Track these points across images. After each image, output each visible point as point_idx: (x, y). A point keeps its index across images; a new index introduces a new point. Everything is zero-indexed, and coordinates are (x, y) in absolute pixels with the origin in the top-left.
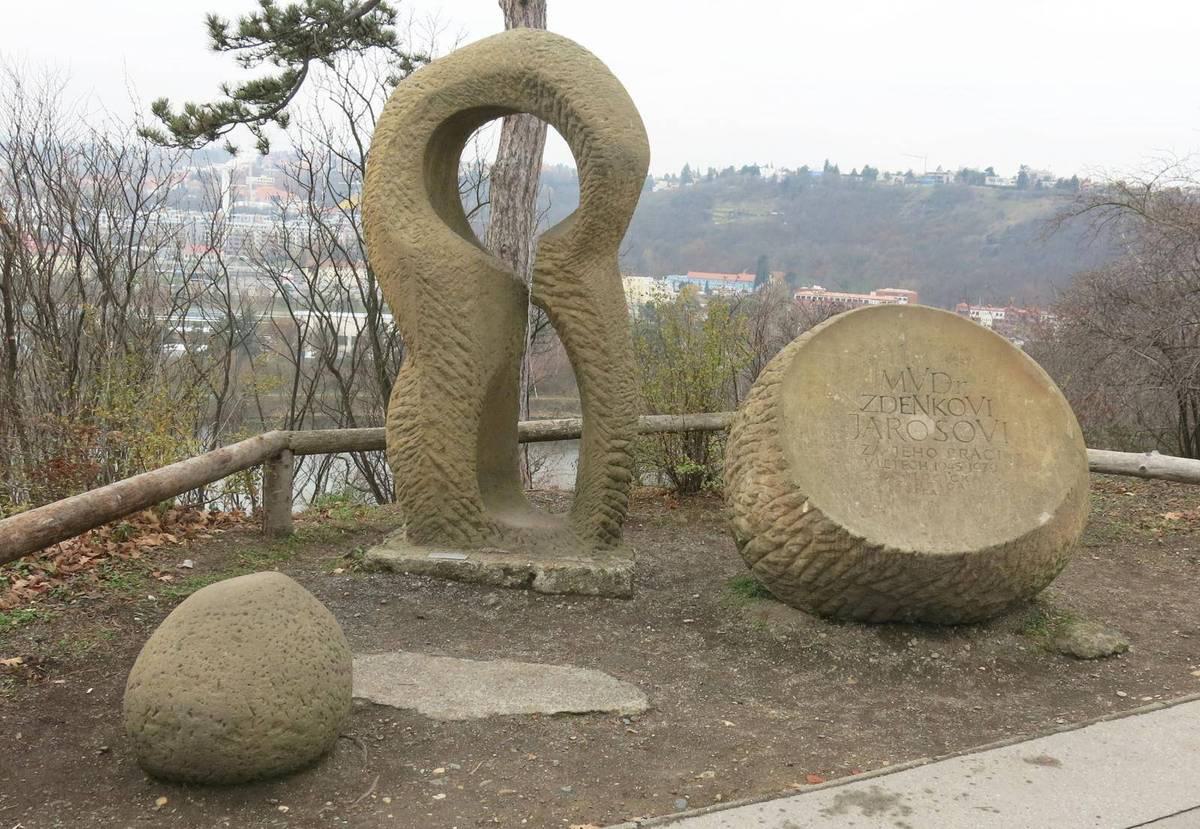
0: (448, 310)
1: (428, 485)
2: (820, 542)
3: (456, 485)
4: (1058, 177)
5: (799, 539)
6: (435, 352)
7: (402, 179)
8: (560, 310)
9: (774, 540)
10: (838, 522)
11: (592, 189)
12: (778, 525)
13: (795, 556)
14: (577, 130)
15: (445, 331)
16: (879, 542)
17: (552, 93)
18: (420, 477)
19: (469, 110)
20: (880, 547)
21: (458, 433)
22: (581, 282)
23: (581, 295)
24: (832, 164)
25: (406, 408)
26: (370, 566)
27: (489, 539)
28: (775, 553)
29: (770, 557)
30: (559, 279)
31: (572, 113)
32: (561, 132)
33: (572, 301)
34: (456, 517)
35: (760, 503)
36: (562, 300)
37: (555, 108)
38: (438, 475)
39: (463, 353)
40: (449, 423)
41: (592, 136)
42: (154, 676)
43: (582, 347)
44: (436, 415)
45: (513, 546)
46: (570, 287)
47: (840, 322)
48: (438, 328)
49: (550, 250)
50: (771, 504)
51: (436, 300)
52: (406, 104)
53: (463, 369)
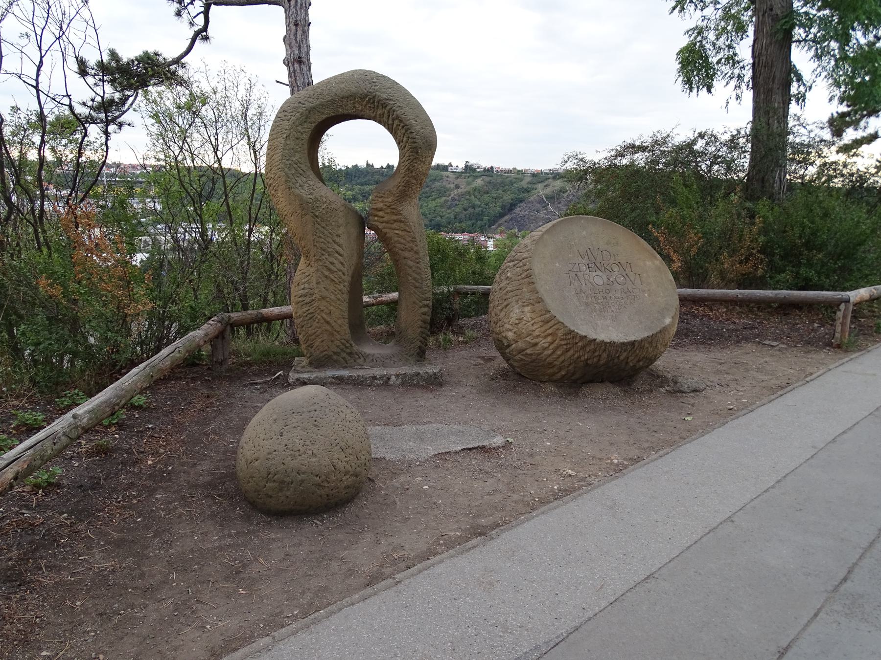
0: (330, 233)
1: (322, 333)
2: (562, 340)
3: (338, 332)
4: (483, 166)
5: (549, 339)
6: (323, 257)
7: (296, 158)
8: (388, 231)
9: (532, 341)
10: (572, 328)
11: (410, 161)
12: (537, 333)
13: (545, 349)
14: (400, 128)
15: (329, 245)
16: (594, 337)
17: (384, 106)
18: (317, 329)
19: (333, 117)
20: (595, 340)
21: (338, 302)
22: (401, 214)
23: (401, 221)
24: (370, 163)
25: (307, 291)
26: (294, 383)
27: (358, 361)
28: (532, 349)
29: (528, 351)
30: (388, 213)
31: (397, 117)
32: (388, 129)
33: (395, 225)
34: (339, 351)
35: (524, 322)
36: (389, 225)
37: (385, 115)
38: (328, 327)
39: (340, 257)
40: (333, 297)
41: (409, 131)
42: (269, 454)
43: (403, 250)
44: (326, 294)
45: (371, 364)
46: (395, 218)
47: (554, 226)
48: (324, 243)
49: (382, 197)
50: (533, 322)
51: (323, 227)
52: (294, 114)
53: (339, 266)
